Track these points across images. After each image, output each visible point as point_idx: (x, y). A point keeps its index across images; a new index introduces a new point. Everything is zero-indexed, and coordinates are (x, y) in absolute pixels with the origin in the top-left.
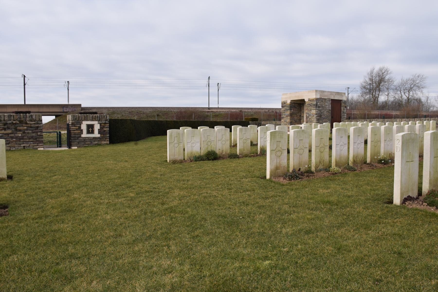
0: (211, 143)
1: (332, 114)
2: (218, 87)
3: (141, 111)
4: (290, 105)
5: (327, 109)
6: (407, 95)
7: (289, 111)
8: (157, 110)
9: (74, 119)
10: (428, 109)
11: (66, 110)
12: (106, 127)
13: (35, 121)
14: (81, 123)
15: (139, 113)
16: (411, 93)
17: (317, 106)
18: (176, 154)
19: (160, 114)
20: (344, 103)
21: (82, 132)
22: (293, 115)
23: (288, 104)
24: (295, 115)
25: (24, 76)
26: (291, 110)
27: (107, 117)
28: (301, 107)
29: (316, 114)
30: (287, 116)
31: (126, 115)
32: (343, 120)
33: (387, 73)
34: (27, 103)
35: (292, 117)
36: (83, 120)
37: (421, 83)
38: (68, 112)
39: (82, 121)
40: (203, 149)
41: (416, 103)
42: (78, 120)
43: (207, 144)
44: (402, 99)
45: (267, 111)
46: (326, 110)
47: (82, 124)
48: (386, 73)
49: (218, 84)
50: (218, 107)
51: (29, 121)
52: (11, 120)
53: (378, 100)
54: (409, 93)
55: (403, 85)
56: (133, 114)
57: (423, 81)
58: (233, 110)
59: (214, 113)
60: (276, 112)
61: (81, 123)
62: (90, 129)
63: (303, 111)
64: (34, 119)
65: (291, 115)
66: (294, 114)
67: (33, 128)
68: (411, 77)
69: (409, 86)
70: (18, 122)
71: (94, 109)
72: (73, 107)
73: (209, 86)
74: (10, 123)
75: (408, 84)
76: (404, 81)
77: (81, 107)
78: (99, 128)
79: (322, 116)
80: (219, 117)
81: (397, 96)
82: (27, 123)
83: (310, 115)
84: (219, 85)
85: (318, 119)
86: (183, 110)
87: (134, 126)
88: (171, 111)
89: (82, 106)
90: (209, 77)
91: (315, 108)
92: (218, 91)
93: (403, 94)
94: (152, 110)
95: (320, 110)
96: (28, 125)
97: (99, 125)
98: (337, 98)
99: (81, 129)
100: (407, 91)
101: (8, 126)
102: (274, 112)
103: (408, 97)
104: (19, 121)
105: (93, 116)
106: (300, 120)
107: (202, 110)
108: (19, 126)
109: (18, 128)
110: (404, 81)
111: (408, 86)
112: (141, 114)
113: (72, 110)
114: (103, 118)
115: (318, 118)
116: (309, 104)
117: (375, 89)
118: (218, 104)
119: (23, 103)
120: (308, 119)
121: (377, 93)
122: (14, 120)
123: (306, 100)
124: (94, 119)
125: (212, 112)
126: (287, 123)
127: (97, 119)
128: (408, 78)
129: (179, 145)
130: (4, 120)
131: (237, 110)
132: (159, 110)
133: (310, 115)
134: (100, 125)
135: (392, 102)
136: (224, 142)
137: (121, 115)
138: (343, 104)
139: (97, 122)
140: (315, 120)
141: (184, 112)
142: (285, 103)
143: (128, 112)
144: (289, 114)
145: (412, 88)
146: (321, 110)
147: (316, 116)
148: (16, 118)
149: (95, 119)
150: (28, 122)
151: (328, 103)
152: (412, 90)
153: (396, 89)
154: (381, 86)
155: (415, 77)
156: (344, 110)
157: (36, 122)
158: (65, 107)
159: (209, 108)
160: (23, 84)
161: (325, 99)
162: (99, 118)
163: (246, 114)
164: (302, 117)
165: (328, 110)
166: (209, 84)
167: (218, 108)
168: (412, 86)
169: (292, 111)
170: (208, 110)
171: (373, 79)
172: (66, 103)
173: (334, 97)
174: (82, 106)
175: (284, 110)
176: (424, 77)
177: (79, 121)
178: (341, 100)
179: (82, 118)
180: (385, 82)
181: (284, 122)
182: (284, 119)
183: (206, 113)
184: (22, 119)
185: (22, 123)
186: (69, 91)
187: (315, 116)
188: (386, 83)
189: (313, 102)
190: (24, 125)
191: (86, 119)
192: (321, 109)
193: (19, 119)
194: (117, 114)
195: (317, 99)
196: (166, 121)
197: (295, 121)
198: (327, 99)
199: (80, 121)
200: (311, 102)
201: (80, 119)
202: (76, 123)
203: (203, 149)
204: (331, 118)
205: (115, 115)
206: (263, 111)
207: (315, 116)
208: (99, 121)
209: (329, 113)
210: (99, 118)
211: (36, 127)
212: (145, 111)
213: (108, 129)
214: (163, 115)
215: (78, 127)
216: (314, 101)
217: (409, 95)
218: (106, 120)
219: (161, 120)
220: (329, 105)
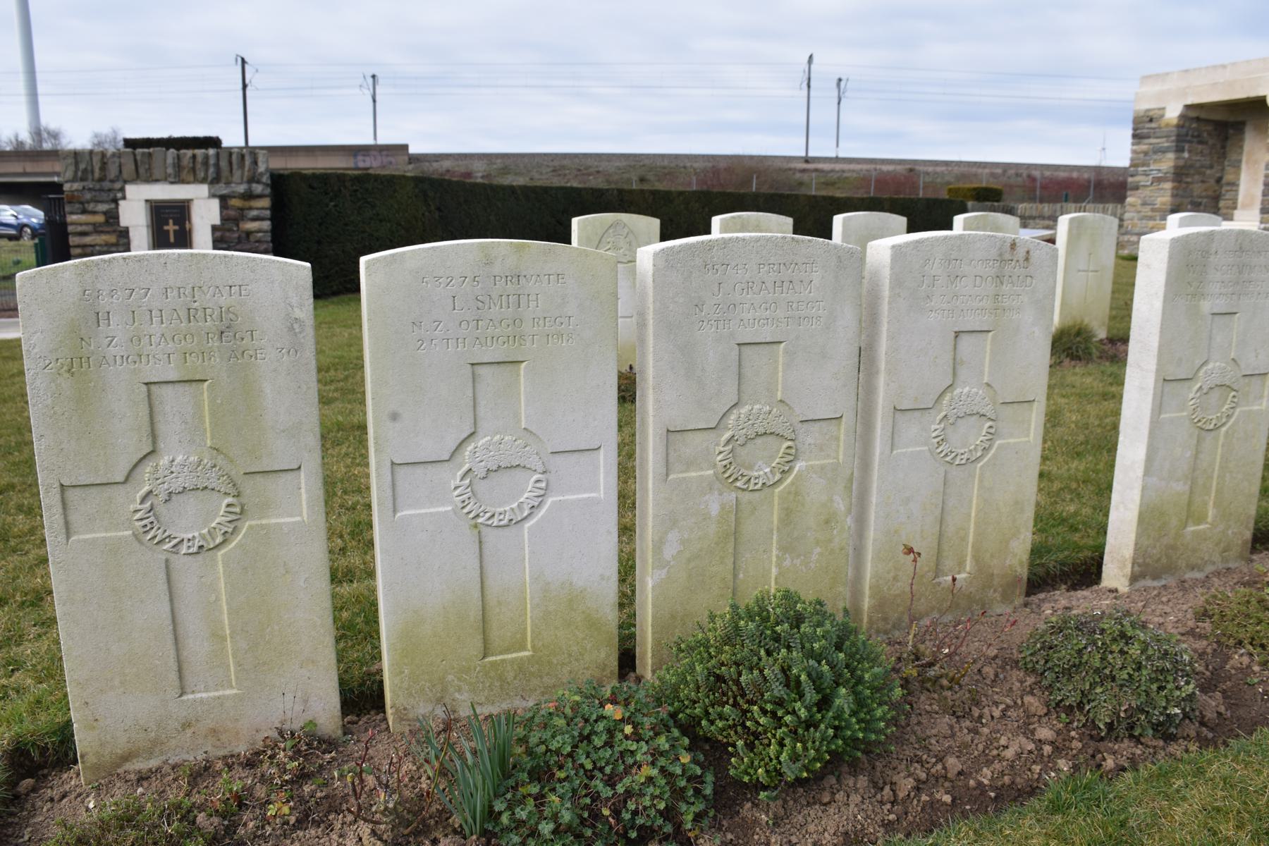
0: (792, 457)
3: (590, 167)
4: (1178, 126)
7: (1171, 156)
8: (641, 164)
9: (76, 172)
11: (364, 161)
12: (255, 213)
14: (119, 195)
15: (585, 172)
18: (197, 648)
19: (648, 177)
21: (123, 241)
22: (1187, 175)
23: (1167, 125)
24: (1197, 177)
25: (243, 61)
26: (1179, 150)
27: (255, 163)
28: (1226, 138)
30: (1159, 180)
31: (544, 177)
35: (1184, 185)
36: (125, 175)
39: (126, 182)
40: (659, 546)
42: (101, 180)
43: (730, 476)
45: (999, 171)
47: (124, 198)
49: (840, 80)
56: (565, 175)
58: (885, 168)
60: (1032, 179)
61: (119, 195)
62: (171, 227)
63: (1234, 157)
65: (1180, 175)
66: (1192, 171)
71: (447, 159)
72: (384, 153)
73: (809, 86)
77: (408, 154)
78: (217, 222)
80: (839, 188)
84: (842, 84)
86: (722, 165)
87: (439, 209)
88: (685, 167)
89: (412, 150)
90: (811, 57)
92: (839, 103)
94: (624, 164)
97: (215, 203)
99: (118, 223)
102: (1024, 175)
105: (194, 157)
107: (786, 166)
112: (589, 175)
113: (382, 162)
114: (235, 166)
118: (837, 146)
124: (184, 174)
125: (816, 170)
126: (1153, 210)
129: (238, 514)
131: (899, 168)
132: (647, 162)
134: (224, 206)
136: (970, 436)
139: (203, 190)
141: (725, 169)
142: (1151, 120)
144: (1172, 170)
149: (193, 170)
158: (362, 153)
159: (807, 160)
160: (240, 86)
162: (211, 170)
163: (928, 179)
164: (1229, 184)
166: (809, 79)
167: (837, 160)
169: (1186, 155)
172: (369, 141)
174: (412, 150)
175: (1146, 153)
177: (106, 185)
181: (1139, 208)
186: (377, 104)
191: (142, 170)
194: (516, 174)
196: (618, 190)
199: (112, 181)
201: (113, 171)
202: (88, 196)
203: (669, 552)
206: (987, 171)
208: (215, 181)
210: (211, 170)
212: (604, 166)
213: (266, 225)
214: (659, 180)
215: (105, 213)
218: (253, 179)
219: (535, 184)
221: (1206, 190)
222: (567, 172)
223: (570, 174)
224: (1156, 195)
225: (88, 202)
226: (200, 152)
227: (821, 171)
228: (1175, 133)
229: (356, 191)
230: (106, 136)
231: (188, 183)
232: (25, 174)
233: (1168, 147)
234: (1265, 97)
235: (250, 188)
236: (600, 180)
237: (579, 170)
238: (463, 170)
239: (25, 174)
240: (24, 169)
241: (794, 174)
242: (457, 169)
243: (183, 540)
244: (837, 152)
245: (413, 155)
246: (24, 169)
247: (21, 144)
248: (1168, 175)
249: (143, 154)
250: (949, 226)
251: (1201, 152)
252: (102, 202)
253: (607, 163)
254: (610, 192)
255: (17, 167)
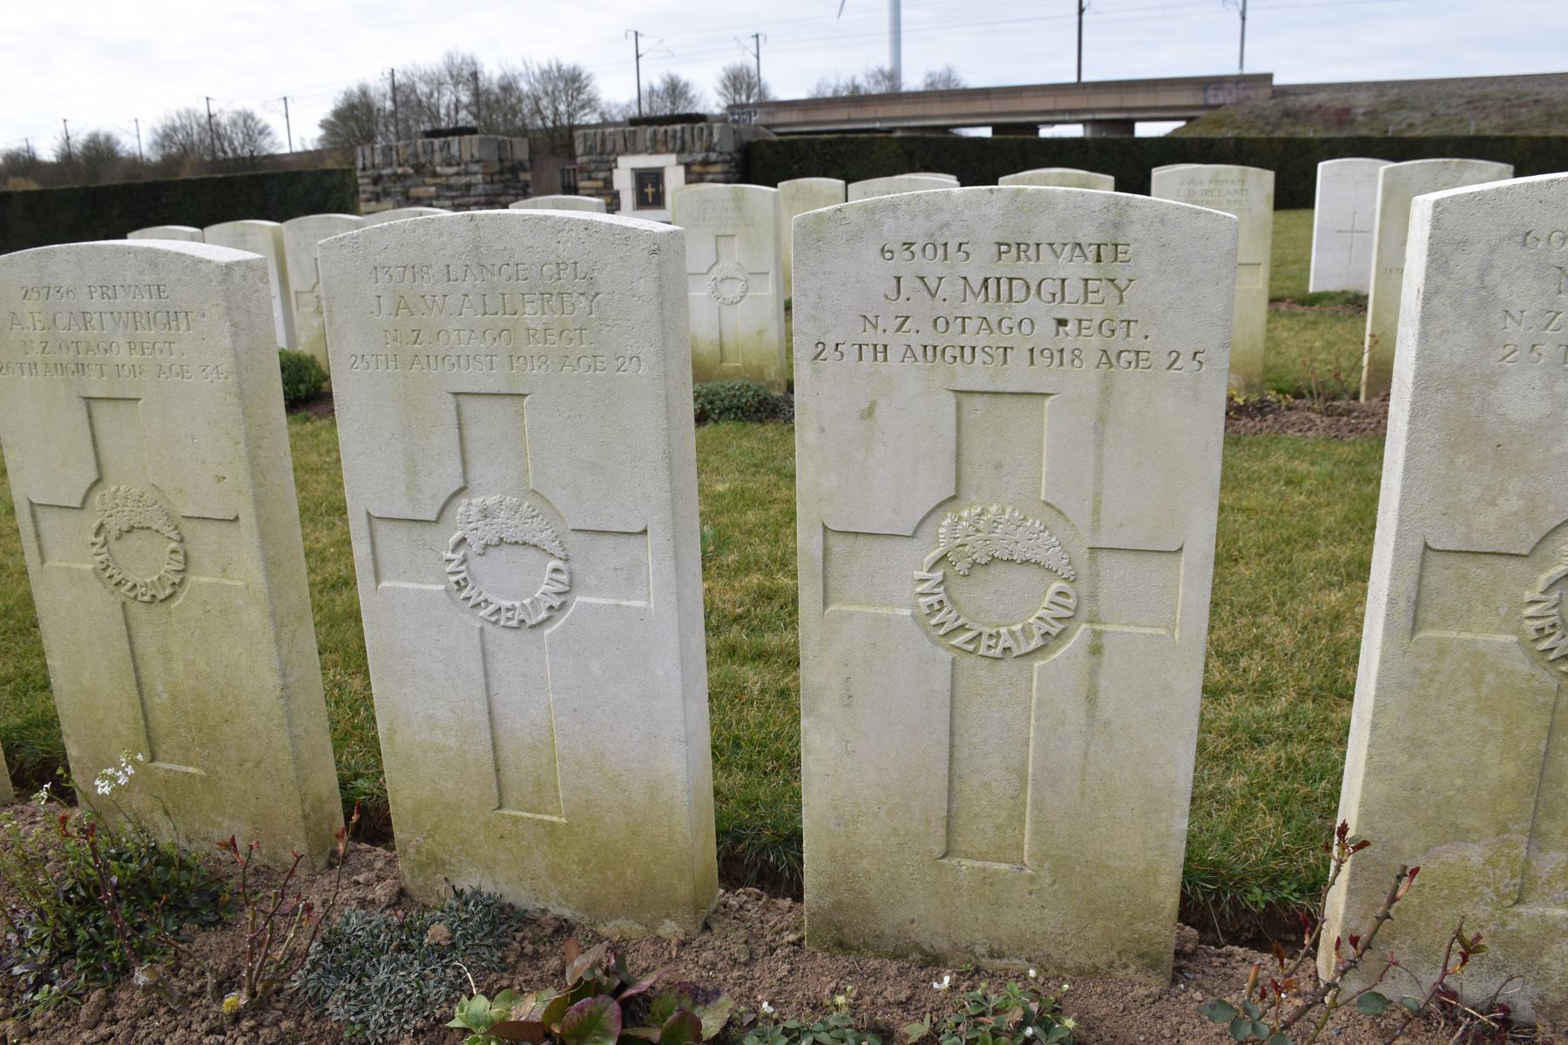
3: (1526, 95)
11: (1216, 96)
12: (710, 177)
13: (458, 164)
15: (1515, 102)
21: (615, 201)
27: (711, 134)
34: (1085, 79)
38: (1223, 108)
39: (618, 154)
42: (602, 153)
47: (616, 167)
51: (441, 166)
52: (390, 165)
56: (1484, 108)
61: (613, 165)
62: (650, 190)
64: (454, 156)
67: (456, 190)
70: (410, 171)
72: (1242, 85)
74: (389, 176)
77: (1272, 87)
82: (435, 175)
89: (1277, 81)
96: (438, 181)
97: (681, 170)
99: (612, 187)
101: (386, 185)
104: (412, 167)
105: (666, 131)
108: (416, 186)
109: (414, 192)
112: (1521, 106)
119: (1073, 79)
122: (400, 165)
124: (659, 147)
127: (671, 146)
130: (373, 166)
137: (1427, 115)
143: (1460, 102)
148: (405, 157)
149: (666, 143)
150: (438, 169)
157: (463, 167)
160: (1076, 10)
164: (261, 133)
172: (1230, 68)
174: (1277, 81)
177: (605, 157)
179: (614, 142)
184: (422, 160)
185: (423, 175)
190: (428, 180)
191: (629, 145)
193: (411, 161)
194: (1413, 108)
199: (609, 154)
201: (609, 147)
202: (593, 166)
205: (1403, 113)
208: (681, 151)
210: (679, 142)
211: (461, 185)
212: (1547, 92)
218: (710, 149)
222: (1489, 103)
223: (1492, 106)
225: (593, 171)
226: (670, 128)
229: (825, 154)
230: (940, 75)
231: (662, 153)
232: (849, 121)
235: (707, 157)
236: (1536, 113)
237: (1509, 100)
238: (1338, 105)
239: (849, 121)
240: (849, 115)
242: (1330, 104)
243: (980, 634)
245: (1279, 87)
246: (849, 115)
247: (856, 88)
249: (630, 132)
250: (776, 186)
252: (602, 171)
254: (1224, 142)
255: (842, 114)
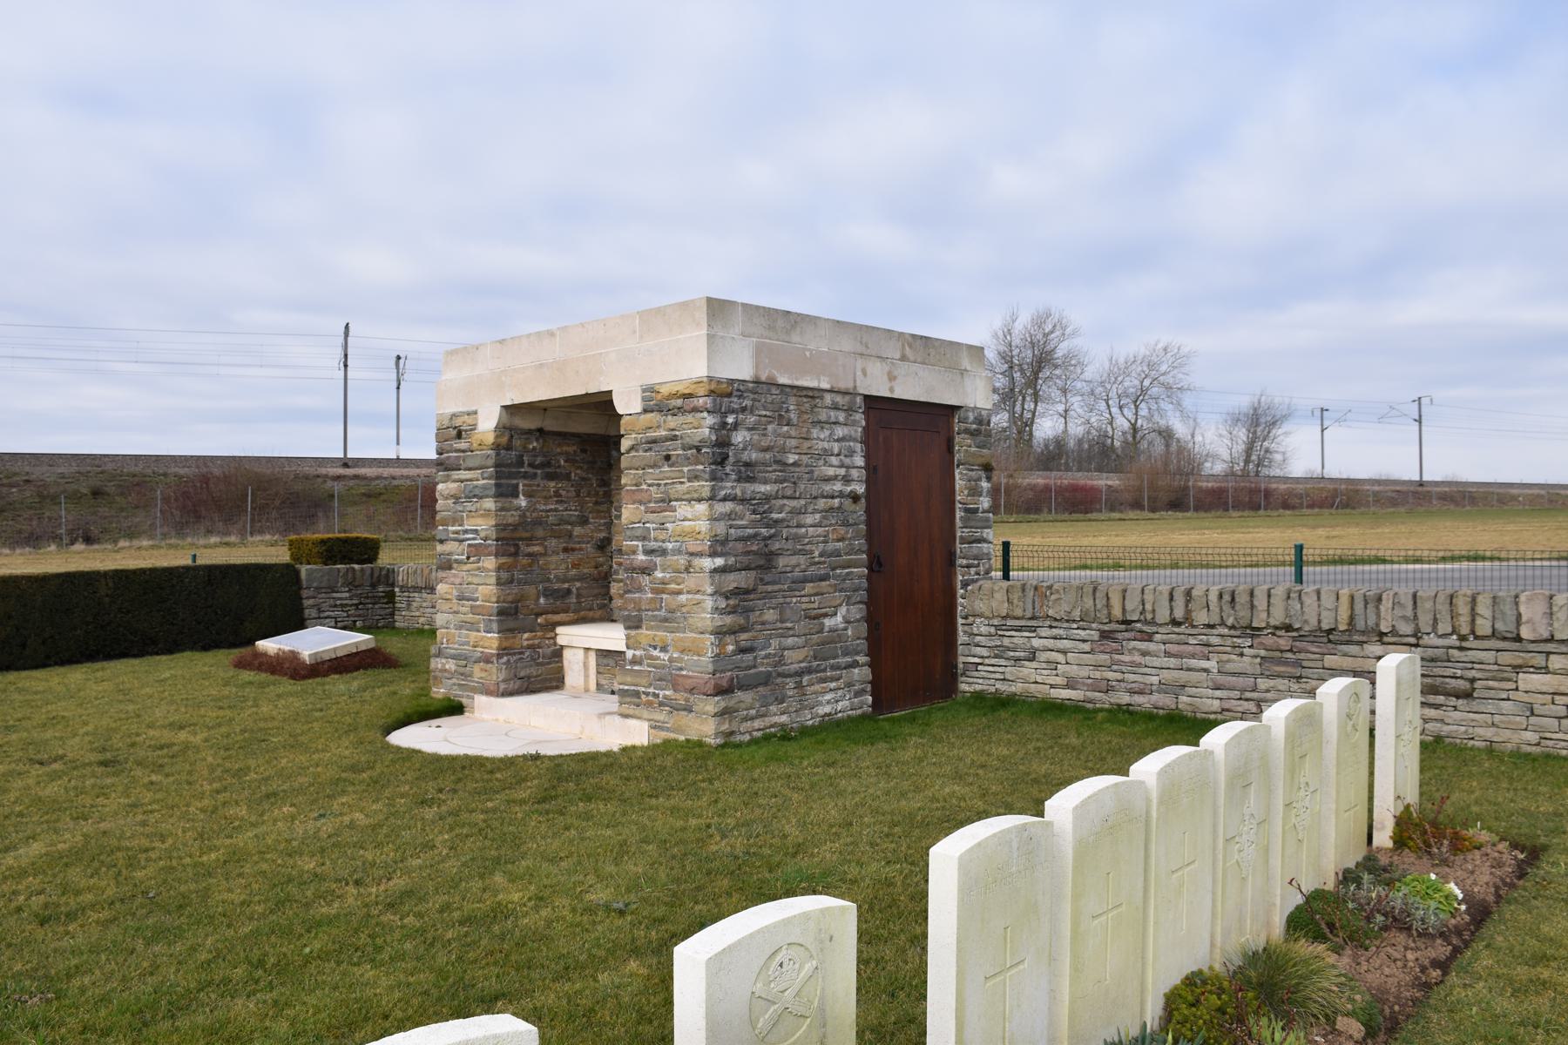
1: (870, 536)
2: (398, 372)
3: (16, 474)
4: (497, 447)
5: (827, 488)
6: (1131, 416)
10: (1199, 465)
16: (1143, 411)
17: (721, 461)
20: (974, 434)
22: (530, 540)
26: (504, 492)
29: (718, 546)
30: (476, 552)
32: (965, 585)
33: (1064, 334)
35: (525, 561)
37: (1175, 372)
41: (1159, 447)
44: (1113, 430)
46: (822, 504)
48: (1057, 333)
49: (399, 358)
50: (398, 459)
53: (1031, 434)
54: (1137, 407)
55: (1116, 379)
57: (1181, 365)
59: (363, 483)
66: (540, 532)
68: (1143, 351)
69: (1137, 383)
73: (346, 366)
75: (1133, 374)
76: (1116, 361)
79: (782, 562)
80: (385, 501)
81: (1097, 417)
83: (664, 552)
84: (402, 361)
85: (737, 592)
91: (704, 487)
92: (398, 388)
93: (1115, 410)
94: (74, 469)
95: (760, 506)
98: (914, 386)
100: (1128, 400)
103: (1133, 421)
106: (603, 579)
107: (307, 469)
110: (1116, 361)
111: (1131, 384)
112: (11, 486)
115: (733, 581)
116: (654, 441)
117: (1020, 392)
118: (398, 444)
120: (640, 589)
121: (1030, 405)
123: (627, 404)
125: (356, 477)
126: (474, 610)
128: (1131, 356)
132: (109, 467)
133: (664, 552)
135: (1080, 442)
138: (963, 446)
140: (709, 603)
142: (459, 436)
145: (1147, 389)
146: (767, 498)
147: (719, 562)
151: (840, 432)
152: (1146, 397)
153: (1092, 393)
154: (1040, 382)
155: (1154, 350)
156: (975, 492)
159: (346, 463)
161: (812, 394)
165: (841, 495)
166: (346, 356)
167: (398, 462)
168: (1147, 383)
169: (522, 502)
170: (341, 471)
171: (1012, 357)
173: (892, 378)
176: (1185, 350)
178: (952, 409)
180: (1056, 367)
182: (458, 574)
183: (329, 484)
187: (708, 563)
188: (1058, 372)
189: (689, 418)
192: (763, 488)
195: (724, 395)
197: (548, 593)
198: (828, 398)
200: (672, 422)
204: (869, 578)
207: (708, 563)
209: (846, 524)
212: (37, 472)
214: (122, 494)
216: (695, 410)
217: (1136, 414)
220: (851, 453)
221: (575, 566)
224: (476, 580)
227: (364, 478)
228: (491, 462)
233: (484, 487)
234: (610, 392)
241: (325, 481)
244: (398, 451)
248: (489, 542)
251: (557, 494)
253: (45, 468)
